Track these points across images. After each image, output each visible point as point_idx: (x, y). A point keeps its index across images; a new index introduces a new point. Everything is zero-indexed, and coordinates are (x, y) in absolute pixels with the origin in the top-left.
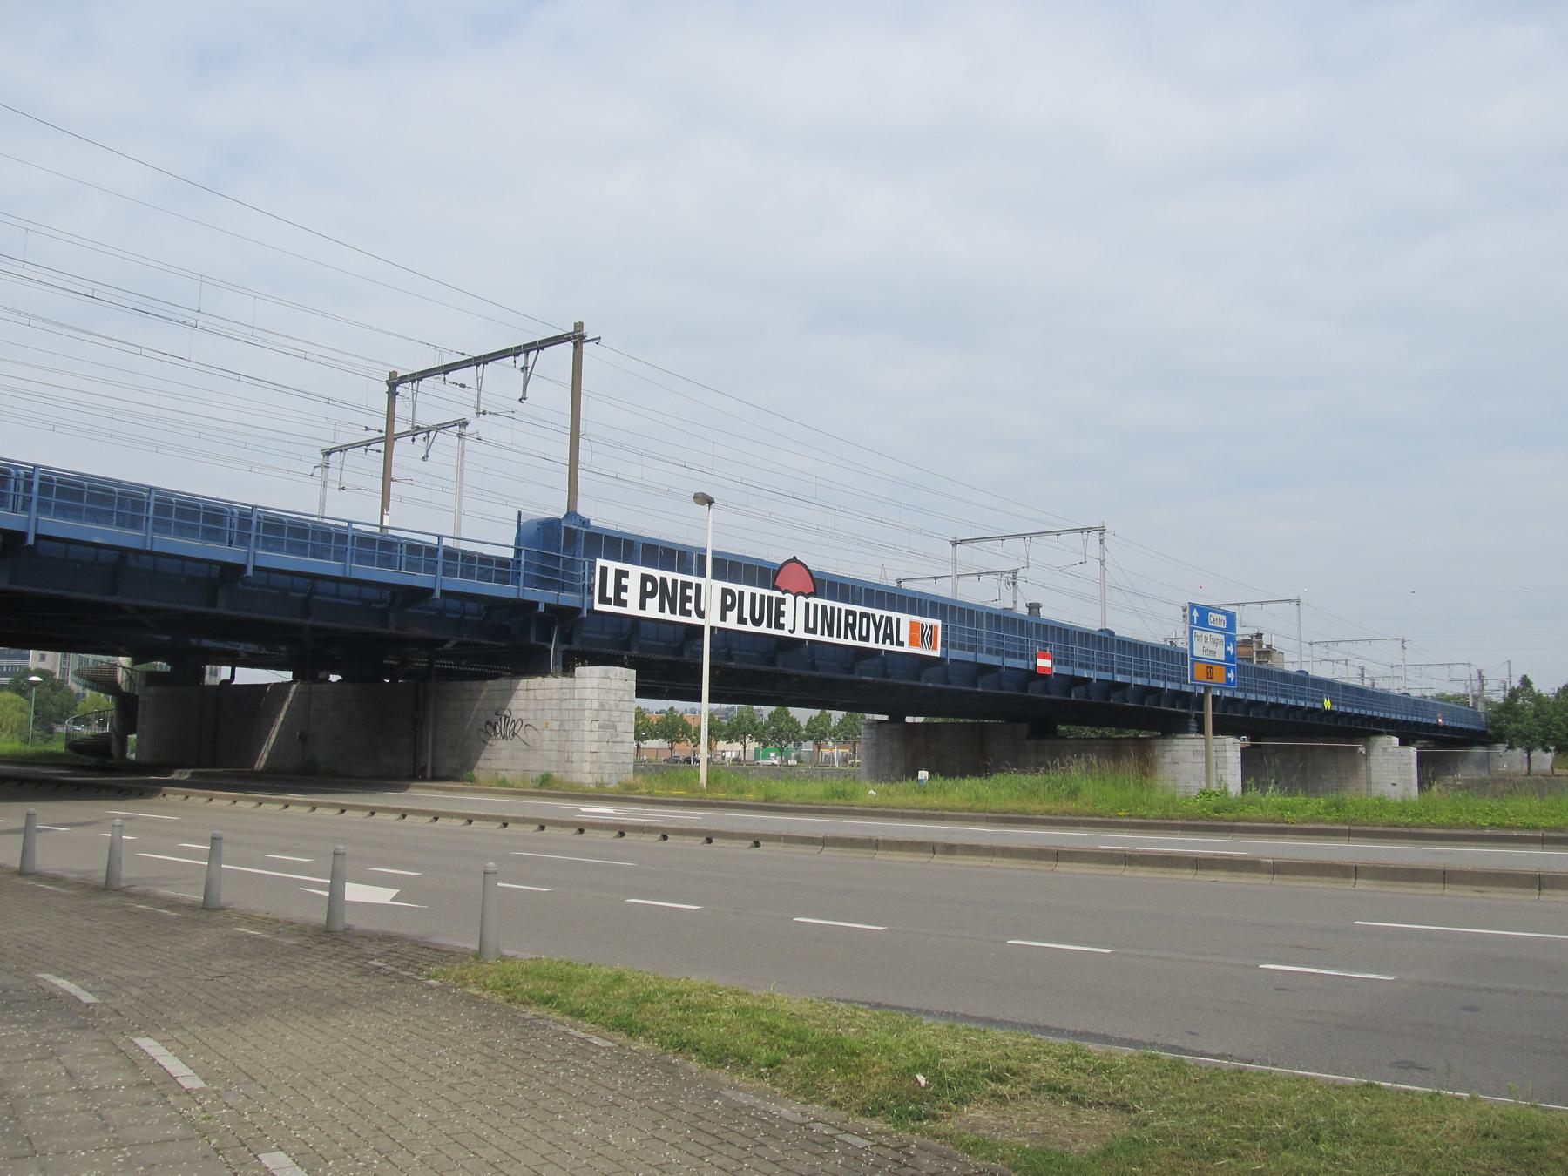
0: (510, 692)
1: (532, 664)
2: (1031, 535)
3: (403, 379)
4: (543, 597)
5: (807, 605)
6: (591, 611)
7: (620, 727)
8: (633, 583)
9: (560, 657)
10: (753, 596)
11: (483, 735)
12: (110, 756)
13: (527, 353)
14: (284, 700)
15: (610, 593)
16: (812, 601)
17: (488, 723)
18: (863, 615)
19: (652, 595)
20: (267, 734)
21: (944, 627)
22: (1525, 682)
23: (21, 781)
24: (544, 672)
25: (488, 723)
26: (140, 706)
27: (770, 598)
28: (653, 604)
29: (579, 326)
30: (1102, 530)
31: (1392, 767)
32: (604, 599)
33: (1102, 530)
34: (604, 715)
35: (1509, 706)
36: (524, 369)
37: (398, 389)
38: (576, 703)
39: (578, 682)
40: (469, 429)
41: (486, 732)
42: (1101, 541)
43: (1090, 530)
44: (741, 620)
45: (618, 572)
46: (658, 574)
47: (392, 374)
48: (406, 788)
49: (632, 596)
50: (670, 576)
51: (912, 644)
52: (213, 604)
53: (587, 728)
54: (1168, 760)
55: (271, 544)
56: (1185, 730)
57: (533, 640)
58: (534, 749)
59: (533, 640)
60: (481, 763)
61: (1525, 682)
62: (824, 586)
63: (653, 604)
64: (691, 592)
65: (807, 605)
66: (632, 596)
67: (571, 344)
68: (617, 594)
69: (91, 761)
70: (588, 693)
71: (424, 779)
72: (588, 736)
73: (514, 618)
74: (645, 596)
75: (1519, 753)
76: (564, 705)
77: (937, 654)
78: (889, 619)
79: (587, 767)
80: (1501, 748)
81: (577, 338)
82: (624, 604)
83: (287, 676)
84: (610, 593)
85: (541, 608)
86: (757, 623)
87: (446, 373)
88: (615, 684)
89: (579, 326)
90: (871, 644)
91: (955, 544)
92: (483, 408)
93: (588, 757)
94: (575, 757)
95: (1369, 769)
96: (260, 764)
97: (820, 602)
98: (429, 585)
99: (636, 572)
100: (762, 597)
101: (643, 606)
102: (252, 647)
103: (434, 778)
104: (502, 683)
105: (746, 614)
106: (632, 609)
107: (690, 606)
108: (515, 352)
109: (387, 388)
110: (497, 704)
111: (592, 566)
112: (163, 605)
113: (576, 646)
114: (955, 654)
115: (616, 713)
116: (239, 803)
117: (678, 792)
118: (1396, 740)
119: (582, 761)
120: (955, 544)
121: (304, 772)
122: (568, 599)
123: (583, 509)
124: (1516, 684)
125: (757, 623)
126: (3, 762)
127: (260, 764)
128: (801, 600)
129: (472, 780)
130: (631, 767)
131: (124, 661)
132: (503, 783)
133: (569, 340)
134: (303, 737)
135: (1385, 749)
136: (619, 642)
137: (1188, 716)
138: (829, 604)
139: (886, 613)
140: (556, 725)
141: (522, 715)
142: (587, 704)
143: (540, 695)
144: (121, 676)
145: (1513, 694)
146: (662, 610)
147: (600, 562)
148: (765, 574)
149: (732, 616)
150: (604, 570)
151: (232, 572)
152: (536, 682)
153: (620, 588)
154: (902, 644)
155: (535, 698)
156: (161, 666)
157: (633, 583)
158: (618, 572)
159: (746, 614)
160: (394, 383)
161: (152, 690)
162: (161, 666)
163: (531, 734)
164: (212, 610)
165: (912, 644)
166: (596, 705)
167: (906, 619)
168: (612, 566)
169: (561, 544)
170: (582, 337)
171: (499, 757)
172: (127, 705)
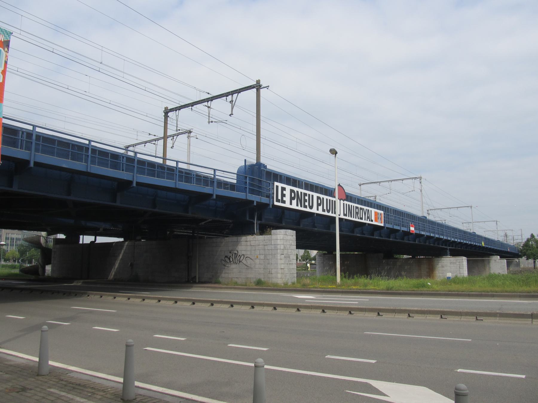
0: (237, 243)
1: (245, 229)
2: (391, 181)
3: (172, 110)
4: (255, 198)
5: (344, 204)
6: (273, 205)
7: (291, 258)
8: (287, 193)
9: (258, 226)
10: (327, 199)
11: (223, 262)
12: (38, 274)
13: (232, 95)
14: (121, 249)
15: (280, 198)
16: (345, 202)
17: (226, 257)
18: (361, 209)
19: (294, 199)
20: (114, 264)
21: (384, 214)
22: (532, 236)
23: (12, 289)
24: (252, 233)
25: (226, 257)
26: (53, 253)
27: (332, 201)
28: (294, 202)
29: (258, 82)
30: (421, 178)
31: (498, 265)
32: (278, 201)
33: (421, 178)
34: (285, 252)
35: (526, 244)
36: (231, 102)
37: (169, 114)
38: (273, 246)
39: (274, 237)
40: (192, 134)
41: (225, 261)
42: (420, 182)
43: (415, 178)
44: (324, 210)
45: (282, 187)
46: (296, 189)
47: (166, 108)
48: (192, 287)
49: (287, 199)
50: (300, 190)
51: (376, 221)
52: (115, 201)
53: (279, 258)
54: (440, 266)
55: (141, 172)
56: (446, 254)
57: (248, 219)
58: (251, 268)
59: (248, 219)
60: (223, 275)
61: (532, 236)
62: (349, 198)
63: (294, 202)
64: (307, 198)
65: (344, 204)
66: (287, 199)
67: (255, 90)
68: (282, 198)
69: (33, 277)
70: (279, 242)
71: (195, 282)
72: (279, 262)
73: (242, 207)
74: (292, 199)
75: (531, 261)
76: (266, 248)
77: (382, 225)
78: (368, 210)
79: (279, 276)
80: (524, 258)
81: (258, 86)
82: (284, 202)
83: (122, 240)
84: (280, 198)
85: (255, 204)
86: (328, 211)
87: (192, 106)
88: (289, 237)
89: (258, 82)
90: (363, 221)
91: (360, 185)
92: (211, 119)
93: (280, 271)
94: (273, 271)
95: (490, 268)
96: (111, 276)
97: (348, 203)
98: (211, 192)
99: (288, 188)
100: (330, 200)
101: (291, 204)
102: (107, 226)
103: (200, 282)
104: (234, 239)
105: (325, 208)
106: (287, 205)
107: (307, 204)
108: (226, 95)
109: (164, 114)
110: (230, 248)
111: (274, 184)
112: (92, 201)
113: (263, 221)
114: (388, 226)
115: (290, 251)
116: (131, 300)
117: (330, 287)
118: (499, 257)
119: (277, 273)
120: (360, 185)
121: (135, 281)
122: (264, 200)
123: (263, 161)
124: (529, 237)
125: (328, 211)
126: (2, 279)
127: (111, 276)
128: (342, 201)
129: (219, 283)
130: (295, 275)
131: (44, 234)
132: (236, 283)
133: (254, 88)
134: (132, 265)
135: (495, 261)
136: (282, 218)
137: (447, 249)
138: (350, 204)
139: (368, 208)
140: (262, 257)
141: (243, 253)
142: (279, 247)
143: (253, 243)
144: (42, 241)
145: (528, 240)
146: (297, 205)
147: (276, 184)
148: (329, 192)
149: (320, 208)
150: (277, 187)
151: (125, 184)
152: (250, 238)
153: (283, 195)
154: (372, 221)
155: (251, 245)
156: (62, 236)
157: (287, 193)
158: (282, 187)
159: (325, 208)
160: (167, 112)
161: (58, 246)
162: (62, 236)
163: (249, 262)
164: (114, 204)
165: (376, 221)
166: (282, 247)
167: (373, 210)
168: (280, 185)
169: (257, 175)
170: (260, 86)
171: (233, 272)
172: (47, 255)
